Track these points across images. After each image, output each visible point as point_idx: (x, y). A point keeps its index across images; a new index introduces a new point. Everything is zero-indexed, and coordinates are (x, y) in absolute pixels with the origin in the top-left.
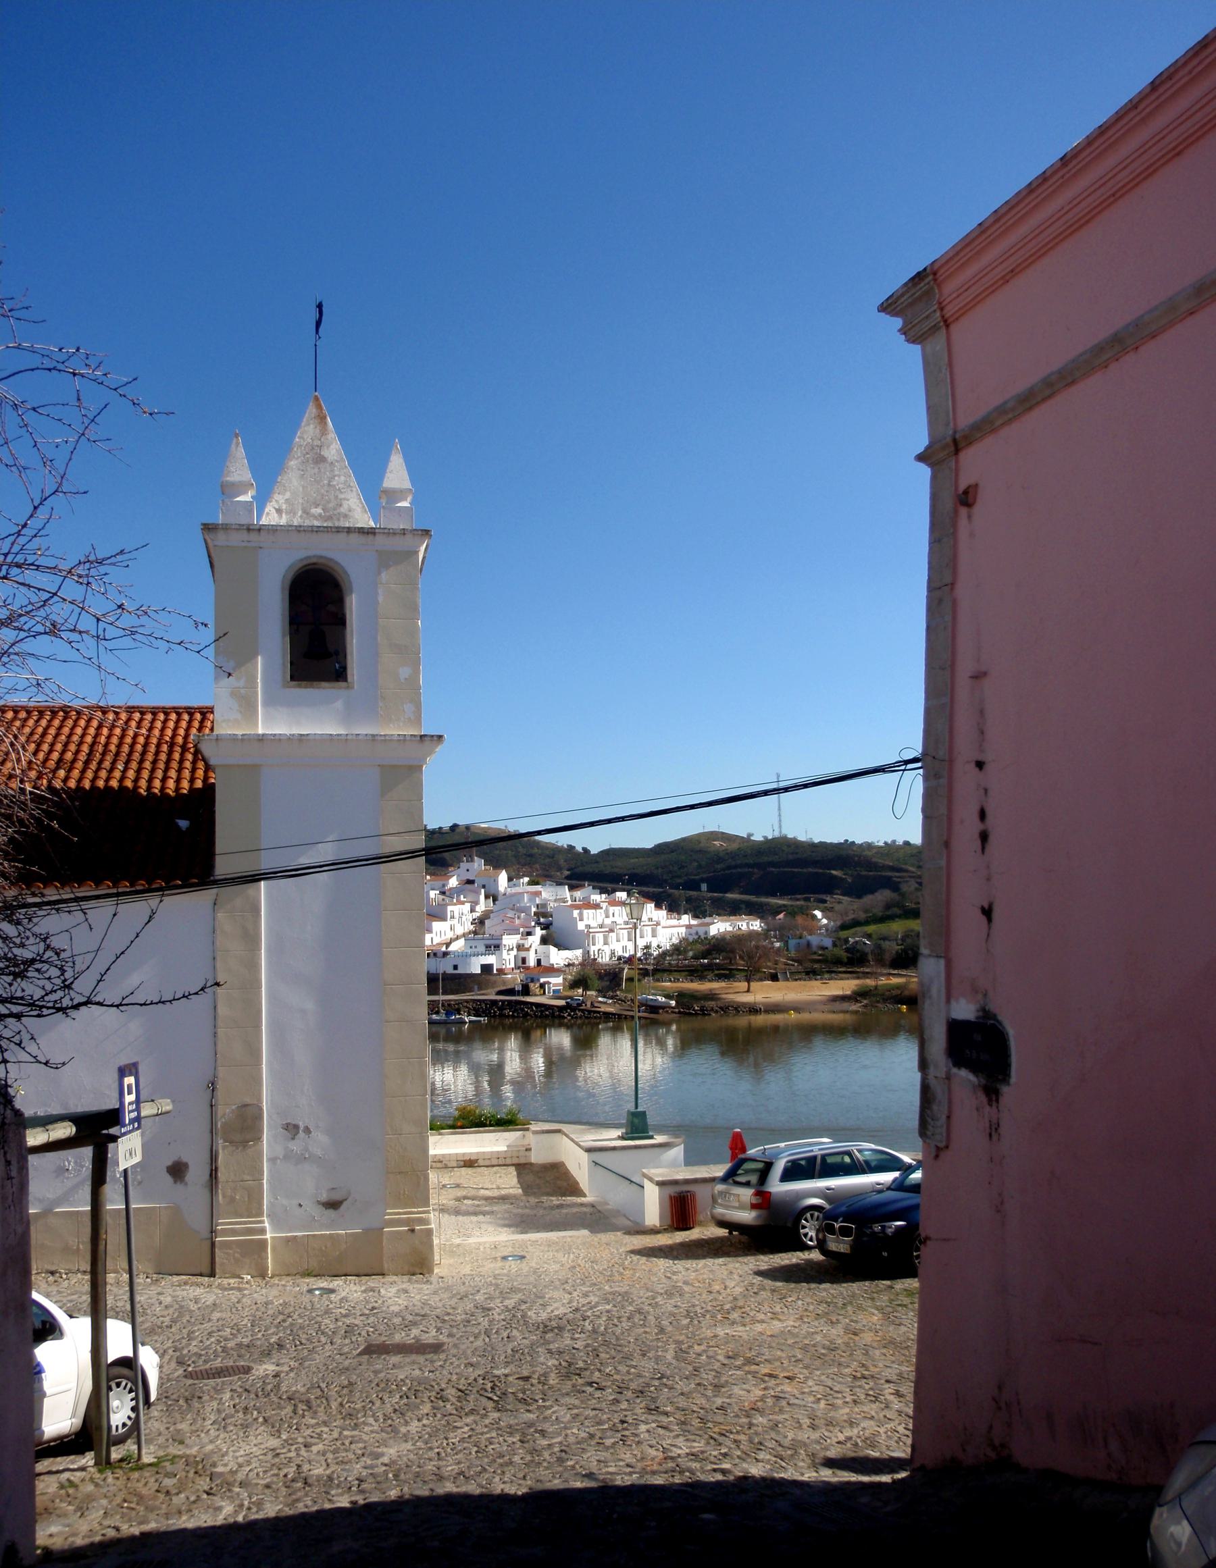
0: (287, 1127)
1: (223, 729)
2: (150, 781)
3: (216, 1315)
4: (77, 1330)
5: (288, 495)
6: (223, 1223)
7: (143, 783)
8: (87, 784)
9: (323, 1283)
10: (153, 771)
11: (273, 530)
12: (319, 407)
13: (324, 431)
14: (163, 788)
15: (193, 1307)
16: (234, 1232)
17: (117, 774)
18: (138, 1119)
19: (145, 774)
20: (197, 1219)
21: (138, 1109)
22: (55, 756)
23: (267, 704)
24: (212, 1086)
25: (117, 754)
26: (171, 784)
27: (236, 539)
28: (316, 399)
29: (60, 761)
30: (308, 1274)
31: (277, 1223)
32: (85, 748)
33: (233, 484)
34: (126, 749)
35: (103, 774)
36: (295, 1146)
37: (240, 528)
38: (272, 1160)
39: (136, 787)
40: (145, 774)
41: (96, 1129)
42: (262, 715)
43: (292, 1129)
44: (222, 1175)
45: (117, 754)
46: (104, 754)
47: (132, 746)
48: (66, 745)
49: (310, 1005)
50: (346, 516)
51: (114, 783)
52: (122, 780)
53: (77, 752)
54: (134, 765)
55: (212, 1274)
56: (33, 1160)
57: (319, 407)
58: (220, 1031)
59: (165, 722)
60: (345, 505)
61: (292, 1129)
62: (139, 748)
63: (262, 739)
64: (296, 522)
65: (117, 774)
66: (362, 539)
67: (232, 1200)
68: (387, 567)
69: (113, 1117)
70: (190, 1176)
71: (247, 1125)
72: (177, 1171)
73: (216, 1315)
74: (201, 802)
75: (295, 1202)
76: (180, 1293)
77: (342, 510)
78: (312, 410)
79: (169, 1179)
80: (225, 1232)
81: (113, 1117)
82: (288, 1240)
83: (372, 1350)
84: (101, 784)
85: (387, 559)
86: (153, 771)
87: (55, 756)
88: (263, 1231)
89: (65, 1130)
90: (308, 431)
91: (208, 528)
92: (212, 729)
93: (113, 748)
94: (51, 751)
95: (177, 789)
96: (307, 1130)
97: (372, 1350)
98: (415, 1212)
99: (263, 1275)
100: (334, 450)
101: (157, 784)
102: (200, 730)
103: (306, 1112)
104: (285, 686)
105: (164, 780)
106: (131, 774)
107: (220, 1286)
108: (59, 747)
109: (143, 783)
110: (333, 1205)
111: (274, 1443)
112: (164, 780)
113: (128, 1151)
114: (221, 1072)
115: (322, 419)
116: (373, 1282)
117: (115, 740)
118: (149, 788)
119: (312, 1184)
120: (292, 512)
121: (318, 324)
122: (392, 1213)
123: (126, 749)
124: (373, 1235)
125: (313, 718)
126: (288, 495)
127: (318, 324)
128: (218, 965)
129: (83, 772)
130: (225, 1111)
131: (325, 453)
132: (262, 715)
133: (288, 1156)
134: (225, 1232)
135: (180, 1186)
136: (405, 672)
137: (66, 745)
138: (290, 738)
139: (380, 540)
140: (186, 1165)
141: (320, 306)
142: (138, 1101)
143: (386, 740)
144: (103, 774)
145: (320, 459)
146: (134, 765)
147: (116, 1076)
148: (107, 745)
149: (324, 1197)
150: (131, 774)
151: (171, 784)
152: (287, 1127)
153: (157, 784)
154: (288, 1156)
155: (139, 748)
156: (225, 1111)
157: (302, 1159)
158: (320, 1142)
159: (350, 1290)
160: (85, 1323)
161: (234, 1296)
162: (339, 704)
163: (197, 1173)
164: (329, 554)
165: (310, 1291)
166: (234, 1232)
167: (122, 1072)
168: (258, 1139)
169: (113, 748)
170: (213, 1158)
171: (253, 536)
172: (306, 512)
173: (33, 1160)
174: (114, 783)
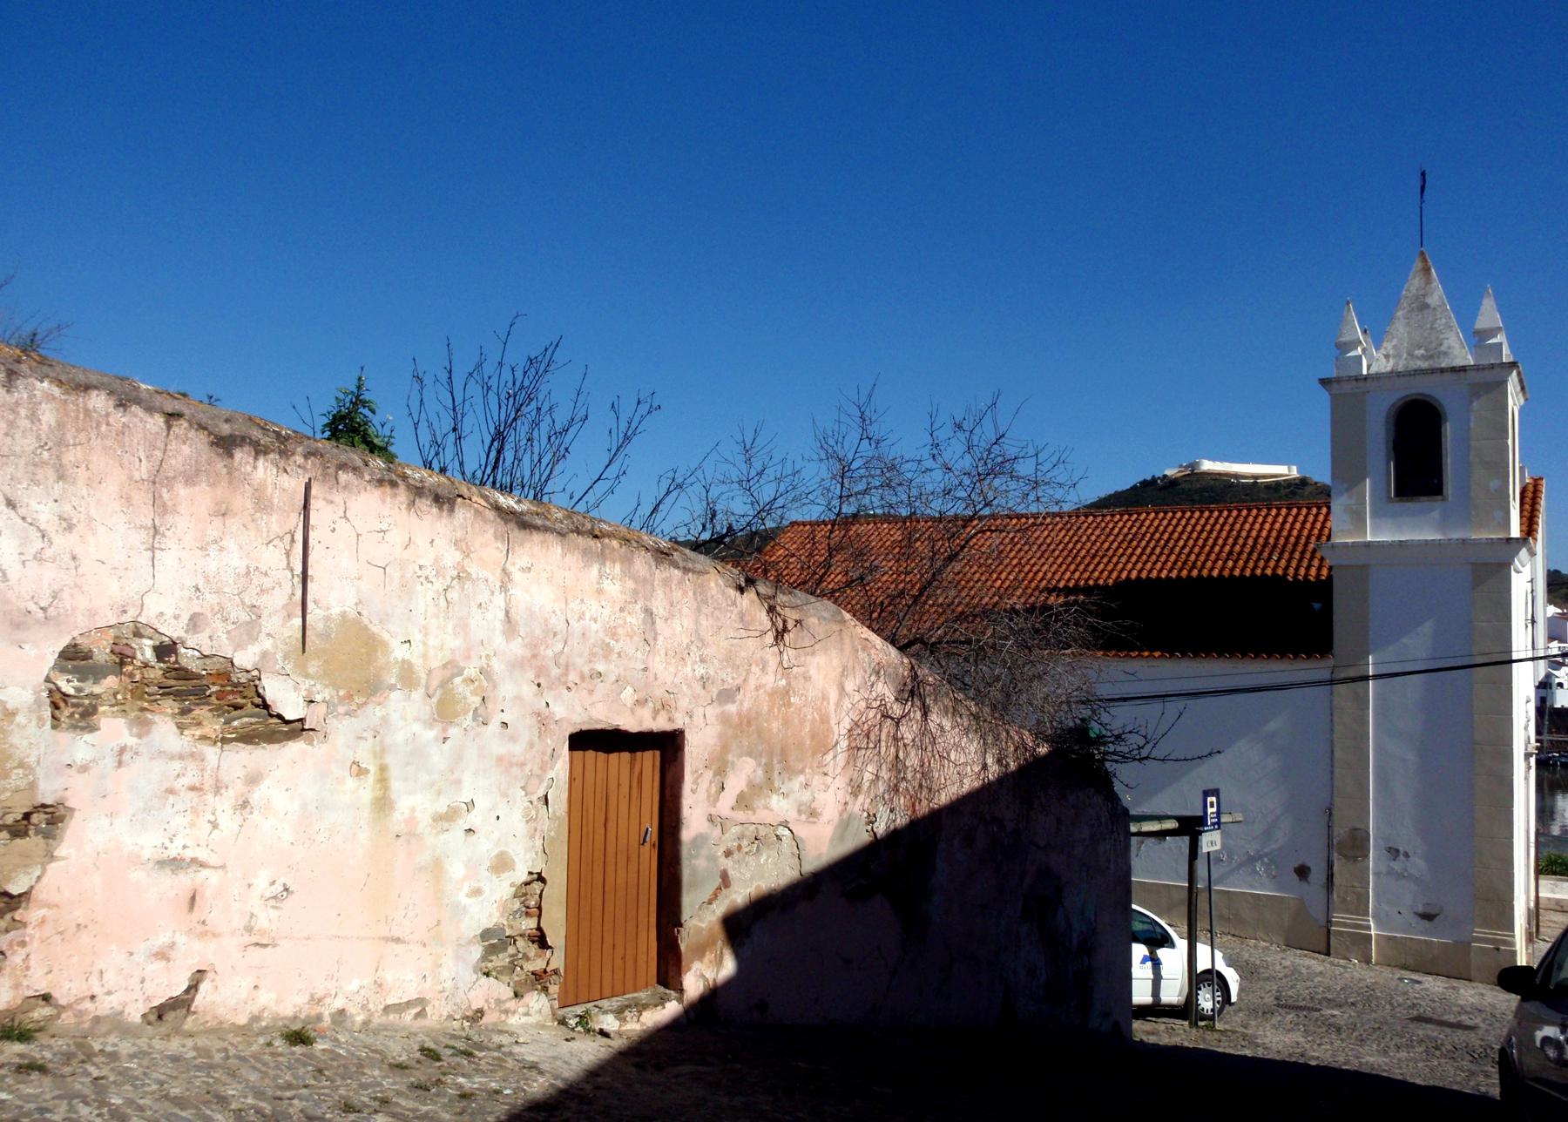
0: (1390, 850)
1: (1338, 539)
2: (1297, 569)
3: (1317, 979)
4: (1182, 944)
5: (1395, 341)
6: (1337, 917)
7: (1291, 571)
8: (1248, 573)
9: (1415, 977)
10: (1300, 560)
11: (1377, 377)
12: (1425, 260)
13: (1429, 281)
14: (1307, 574)
15: (1304, 971)
16: (1345, 925)
17: (1272, 564)
18: (1219, 823)
19: (1294, 563)
20: (1317, 912)
21: (1218, 817)
22: (1227, 548)
23: (1374, 515)
24: (1330, 812)
25: (1275, 546)
26: (1313, 571)
27: (1348, 388)
28: (1422, 253)
29: (1231, 552)
30: (1405, 967)
31: (1379, 925)
32: (1250, 542)
33: (1345, 344)
34: (1282, 541)
35: (1261, 564)
36: (1397, 866)
37: (1350, 379)
38: (1377, 874)
39: (1286, 574)
40: (1294, 563)
41: (1191, 827)
42: (1369, 525)
43: (1394, 852)
44: (1337, 881)
45: (1275, 546)
46: (1264, 546)
47: (1287, 538)
48: (1236, 540)
49: (1411, 756)
50: (1445, 353)
51: (1269, 572)
52: (1274, 569)
53: (1244, 545)
54: (1286, 555)
55: (1328, 954)
56: (1134, 840)
57: (1425, 260)
58: (1337, 771)
59: (1317, 515)
60: (1446, 343)
61: (1394, 852)
62: (1292, 540)
63: (1368, 545)
64: (1401, 368)
65: (1272, 564)
66: (1454, 376)
67: (1344, 900)
68: (1478, 397)
69: (1201, 821)
70: (1313, 877)
71: (1356, 845)
72: (1302, 872)
73: (1317, 979)
74: (1324, 589)
75: (1396, 910)
76: (1298, 960)
77: (1442, 349)
78: (1418, 265)
79: (1295, 876)
80: (1338, 924)
81: (1201, 821)
82: (1390, 938)
83: (1421, 1019)
84: (1258, 572)
85: (1477, 390)
86: (1300, 560)
87: (1227, 548)
88: (1369, 928)
89: (1171, 825)
90: (1415, 283)
91: (1325, 382)
92: (1329, 537)
93: (1272, 541)
94: (1224, 544)
95: (1318, 575)
96: (1406, 855)
97: (1421, 1019)
98: (1500, 935)
99: (1368, 961)
100: (1437, 295)
101: (1302, 571)
102: (1319, 538)
103: (1406, 838)
104: (1389, 500)
105: (1308, 568)
106: (1283, 563)
107: (1332, 964)
108: (1231, 541)
109: (1291, 571)
110: (1428, 917)
111: (1301, 1040)
112: (1308, 568)
113: (1210, 842)
114: (1337, 801)
115: (1427, 270)
116: (1455, 983)
117: (1274, 534)
118: (1296, 574)
119: (1410, 898)
120: (1398, 356)
121: (1423, 188)
122: (1479, 932)
123: (1282, 541)
124: (1463, 947)
125: (1415, 528)
126: (1395, 341)
127: (1423, 188)
128: (1336, 719)
129: (1246, 562)
130: (1340, 832)
131: (1429, 300)
132: (1369, 525)
133: (1390, 872)
134: (1338, 924)
135: (1304, 884)
136: (1494, 484)
137: (1236, 540)
138: (1392, 544)
139: (1471, 375)
140: (1309, 869)
141: (1423, 174)
142: (1218, 813)
143: (1475, 543)
144: (1261, 564)
145: (1424, 307)
146: (1286, 555)
147: (1201, 796)
148: (1268, 537)
149: (1420, 909)
150: (1283, 563)
151: (1313, 571)
152: (1390, 850)
153: (1302, 571)
154: (1390, 872)
155: (1292, 540)
156: (1340, 832)
157: (1400, 876)
158: (1418, 864)
159: (1435, 985)
160: (1185, 942)
161: (1338, 970)
162: (1436, 514)
163: (1318, 875)
164: (1427, 391)
165: (1401, 979)
166: (1345, 925)
167: (1206, 794)
168: (1366, 856)
169: (1272, 541)
170: (1330, 866)
171: (1361, 384)
172: (1410, 355)
173: (1134, 840)
174: (1269, 572)
